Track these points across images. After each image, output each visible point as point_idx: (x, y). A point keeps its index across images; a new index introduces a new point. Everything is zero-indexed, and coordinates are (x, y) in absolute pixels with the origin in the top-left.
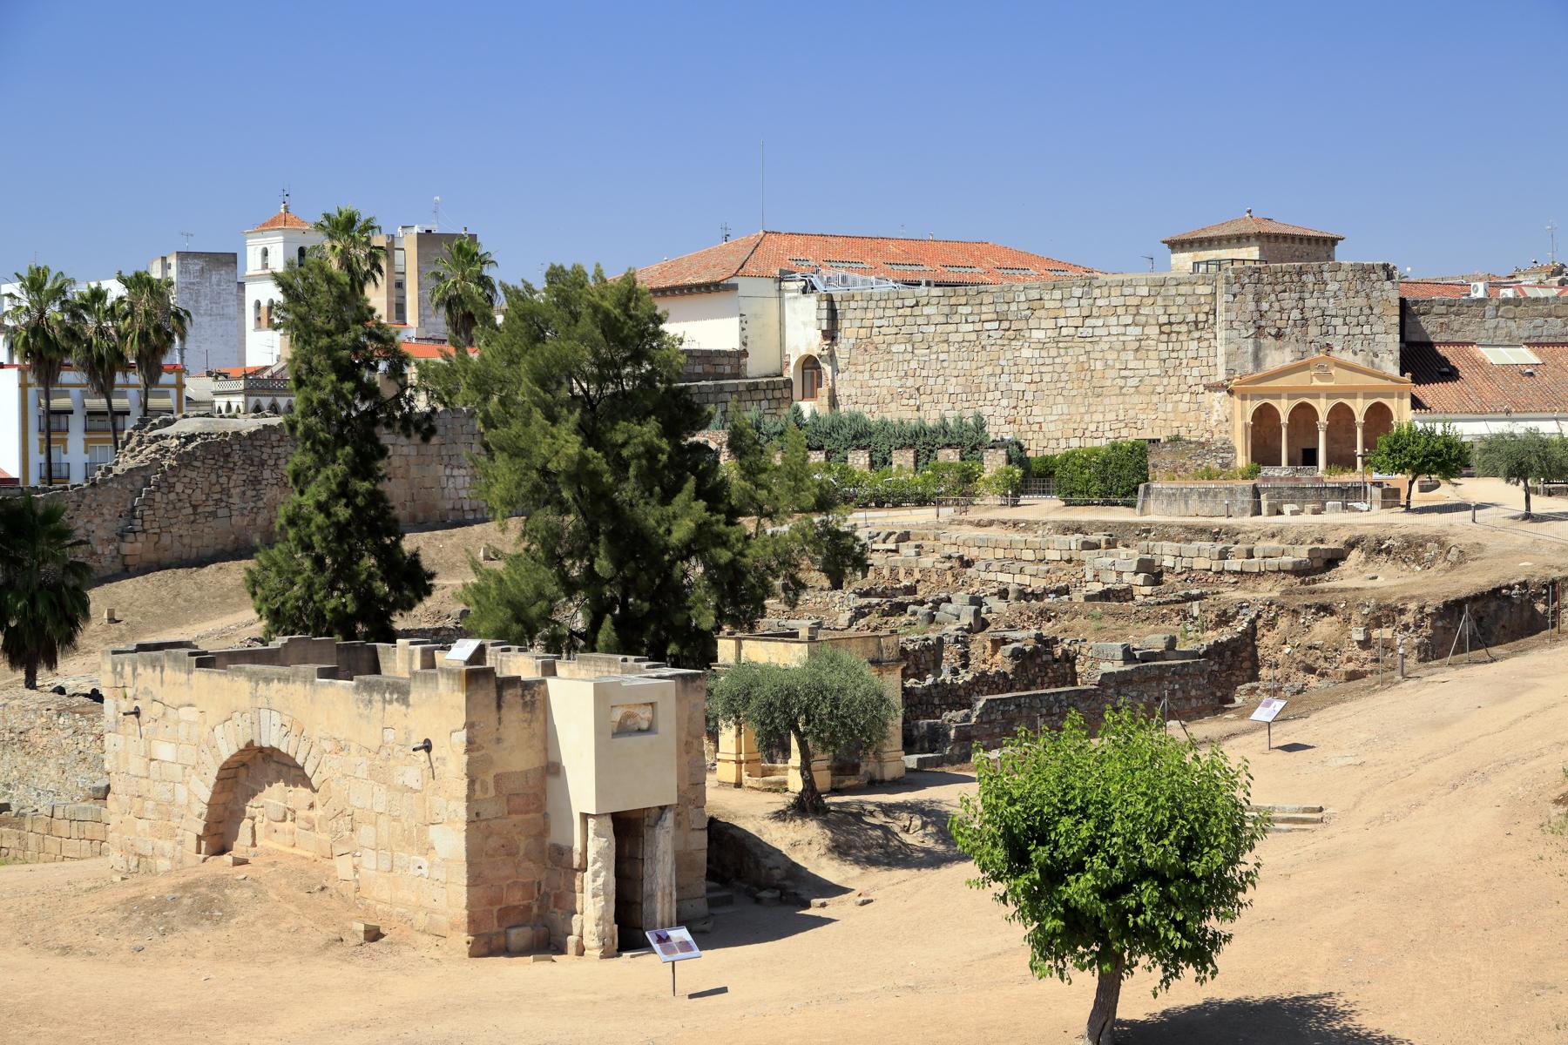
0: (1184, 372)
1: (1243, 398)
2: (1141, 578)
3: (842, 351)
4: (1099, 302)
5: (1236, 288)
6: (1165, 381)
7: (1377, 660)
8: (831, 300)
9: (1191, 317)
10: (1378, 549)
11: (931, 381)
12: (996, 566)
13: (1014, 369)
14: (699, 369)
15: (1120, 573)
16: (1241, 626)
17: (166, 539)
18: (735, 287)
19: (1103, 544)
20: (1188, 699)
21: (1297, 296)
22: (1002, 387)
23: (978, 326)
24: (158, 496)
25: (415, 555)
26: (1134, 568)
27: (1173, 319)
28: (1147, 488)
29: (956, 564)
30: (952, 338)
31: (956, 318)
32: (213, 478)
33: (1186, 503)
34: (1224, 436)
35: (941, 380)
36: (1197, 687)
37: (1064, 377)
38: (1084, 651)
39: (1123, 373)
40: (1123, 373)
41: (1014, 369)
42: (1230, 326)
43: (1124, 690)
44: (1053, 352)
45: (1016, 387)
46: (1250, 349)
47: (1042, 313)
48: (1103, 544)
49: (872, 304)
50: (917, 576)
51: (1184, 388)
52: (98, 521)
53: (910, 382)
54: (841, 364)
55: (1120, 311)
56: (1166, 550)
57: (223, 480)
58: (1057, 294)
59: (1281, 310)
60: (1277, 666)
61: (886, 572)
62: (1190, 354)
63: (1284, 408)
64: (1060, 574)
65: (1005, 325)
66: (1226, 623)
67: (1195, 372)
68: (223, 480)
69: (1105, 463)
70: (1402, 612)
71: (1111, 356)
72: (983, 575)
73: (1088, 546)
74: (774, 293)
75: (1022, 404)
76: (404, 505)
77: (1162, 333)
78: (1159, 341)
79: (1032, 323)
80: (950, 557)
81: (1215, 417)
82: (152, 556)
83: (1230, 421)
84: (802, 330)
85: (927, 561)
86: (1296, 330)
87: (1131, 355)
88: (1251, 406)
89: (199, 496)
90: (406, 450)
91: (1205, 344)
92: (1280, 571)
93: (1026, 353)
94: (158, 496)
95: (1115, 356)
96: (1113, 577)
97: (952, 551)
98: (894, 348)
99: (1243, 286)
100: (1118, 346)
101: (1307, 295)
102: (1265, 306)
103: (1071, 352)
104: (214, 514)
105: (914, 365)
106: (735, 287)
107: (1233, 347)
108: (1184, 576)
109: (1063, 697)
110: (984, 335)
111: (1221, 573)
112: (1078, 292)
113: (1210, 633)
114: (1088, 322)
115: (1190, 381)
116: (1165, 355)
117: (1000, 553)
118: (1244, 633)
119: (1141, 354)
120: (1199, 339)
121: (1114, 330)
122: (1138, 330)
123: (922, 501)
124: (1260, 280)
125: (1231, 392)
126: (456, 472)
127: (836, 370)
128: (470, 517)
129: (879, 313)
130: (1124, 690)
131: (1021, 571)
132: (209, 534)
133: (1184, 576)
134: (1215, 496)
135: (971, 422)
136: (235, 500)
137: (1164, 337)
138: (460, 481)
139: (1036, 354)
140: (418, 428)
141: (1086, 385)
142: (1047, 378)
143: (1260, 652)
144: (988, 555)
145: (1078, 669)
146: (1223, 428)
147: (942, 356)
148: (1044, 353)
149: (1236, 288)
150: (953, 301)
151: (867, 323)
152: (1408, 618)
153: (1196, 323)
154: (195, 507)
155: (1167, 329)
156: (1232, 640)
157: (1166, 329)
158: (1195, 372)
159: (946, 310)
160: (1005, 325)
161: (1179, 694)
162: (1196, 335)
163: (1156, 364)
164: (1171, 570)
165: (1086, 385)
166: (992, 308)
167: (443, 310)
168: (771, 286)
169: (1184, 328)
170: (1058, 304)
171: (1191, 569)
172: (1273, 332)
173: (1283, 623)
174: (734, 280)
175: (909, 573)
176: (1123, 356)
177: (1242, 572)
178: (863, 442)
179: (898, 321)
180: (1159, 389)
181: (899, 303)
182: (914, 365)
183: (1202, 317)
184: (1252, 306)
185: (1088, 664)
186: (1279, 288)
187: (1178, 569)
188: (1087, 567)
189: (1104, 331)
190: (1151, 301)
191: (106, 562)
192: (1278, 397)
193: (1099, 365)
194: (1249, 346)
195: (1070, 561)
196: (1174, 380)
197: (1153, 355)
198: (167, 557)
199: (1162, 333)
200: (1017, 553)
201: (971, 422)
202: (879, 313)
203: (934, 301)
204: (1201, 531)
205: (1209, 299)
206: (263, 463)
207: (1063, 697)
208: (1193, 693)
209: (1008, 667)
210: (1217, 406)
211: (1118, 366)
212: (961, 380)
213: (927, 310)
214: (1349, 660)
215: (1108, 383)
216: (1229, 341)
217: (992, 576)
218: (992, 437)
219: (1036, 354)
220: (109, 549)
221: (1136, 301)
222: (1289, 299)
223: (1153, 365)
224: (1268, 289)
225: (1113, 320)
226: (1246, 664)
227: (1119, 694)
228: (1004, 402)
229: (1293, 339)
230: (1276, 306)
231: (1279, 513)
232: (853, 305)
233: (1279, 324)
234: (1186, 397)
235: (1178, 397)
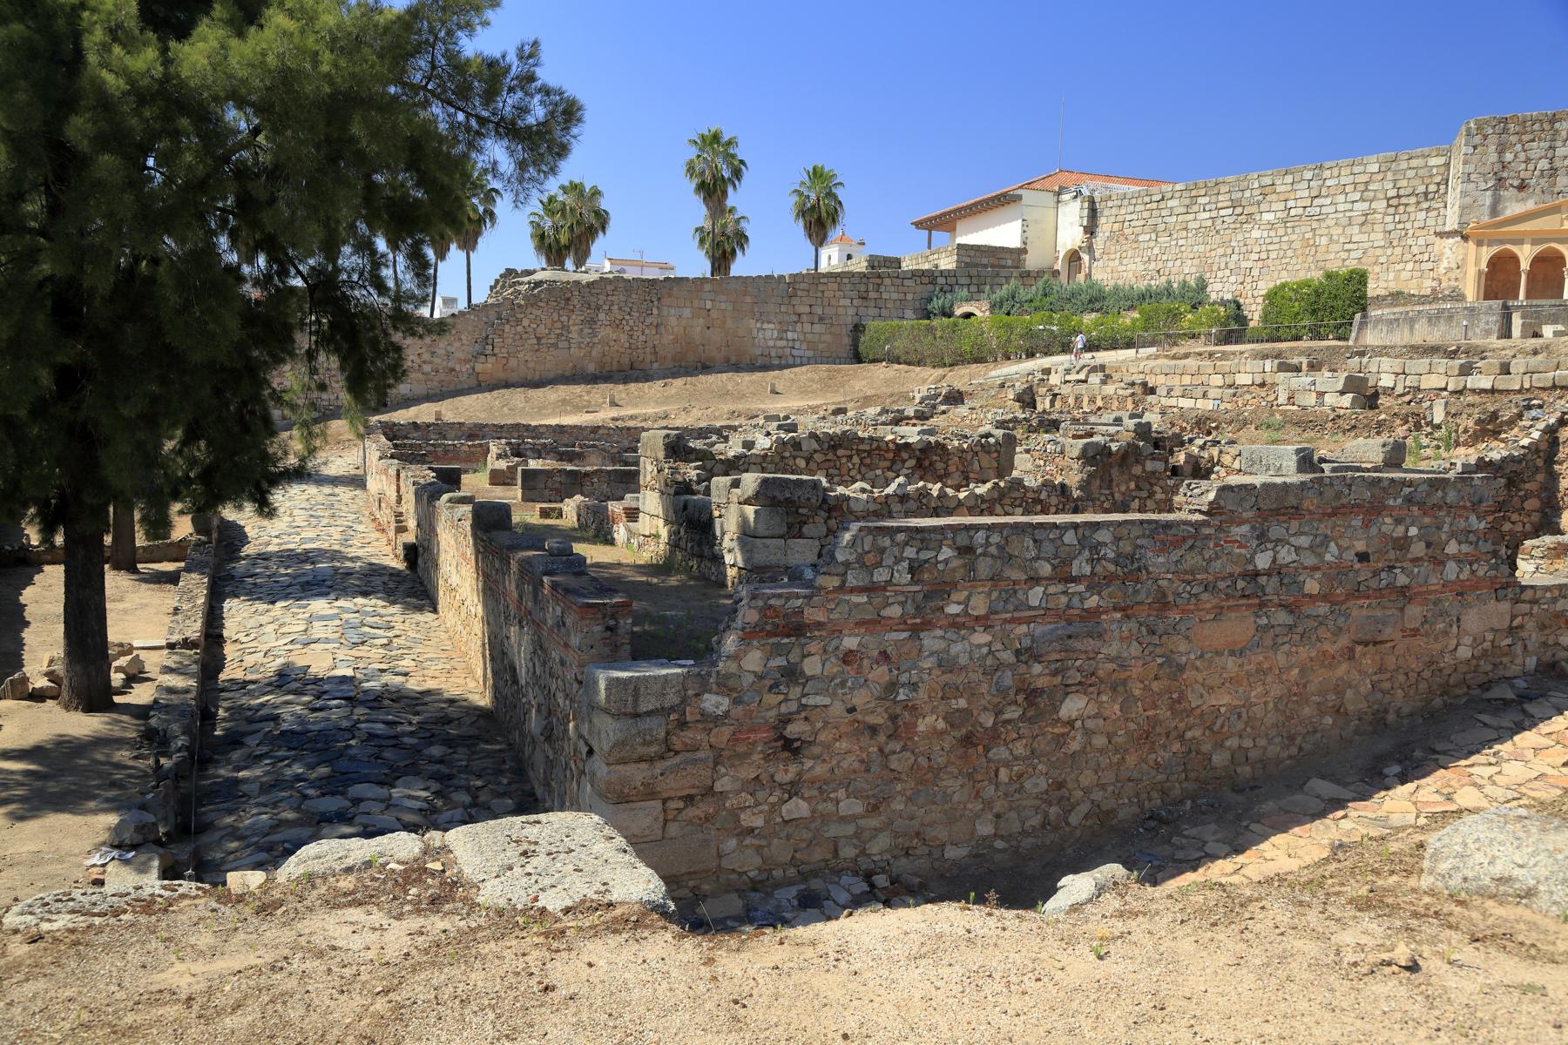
0: (1410, 242)
1: (1479, 244)
2: (1347, 400)
3: (1099, 243)
4: (1328, 183)
5: (1477, 140)
6: (1389, 252)
8: (1092, 201)
9: (1422, 189)
11: (1170, 264)
12: (1177, 392)
13: (1244, 249)
14: (985, 261)
15: (1321, 394)
16: (1528, 436)
17: (513, 363)
18: (1020, 198)
19: (1304, 367)
20: (1439, 562)
21: (1547, 144)
22: (1231, 266)
23: (1214, 214)
24: (507, 327)
26: (1340, 386)
27: (1402, 192)
28: (1364, 317)
29: (1138, 390)
30: (1192, 225)
31: (1195, 208)
32: (555, 316)
33: (1412, 328)
34: (1453, 283)
35: (1178, 263)
36: (1463, 536)
37: (1289, 253)
38: (1227, 459)
39: (1347, 247)
40: (1347, 247)
41: (1244, 249)
42: (1468, 178)
43: (1276, 531)
44: (1281, 232)
45: (1244, 264)
46: (1488, 202)
47: (1274, 197)
48: (1304, 367)
49: (1126, 202)
50: (1099, 403)
51: (1408, 257)
52: (457, 344)
53: (1153, 266)
54: (1097, 255)
55: (1348, 189)
56: (1384, 367)
57: (564, 319)
58: (1289, 179)
59: (1528, 161)
61: (1071, 401)
62: (1417, 224)
63: (1525, 255)
64: (1248, 397)
65: (1238, 210)
66: (1495, 434)
67: (1421, 241)
68: (564, 319)
69: (1318, 294)
71: (1336, 231)
72: (1163, 401)
73: (1284, 367)
74: (1053, 204)
75: (1249, 280)
76: (719, 349)
77: (1389, 206)
78: (1386, 214)
79: (1264, 207)
80: (1133, 384)
81: (1444, 264)
82: (501, 375)
83: (1463, 266)
84: (1070, 233)
85: (1109, 389)
86: (1542, 181)
87: (1356, 229)
88: (1487, 253)
89: (542, 330)
90: (723, 306)
91: (1434, 213)
92: (1554, 387)
93: (1256, 234)
94: (507, 327)
95: (1340, 230)
96: (1311, 400)
97: (1138, 379)
98: (1141, 238)
99: (1485, 137)
100: (1344, 221)
101: (1559, 144)
102: (1509, 156)
103: (1297, 230)
104: (555, 346)
105: (1156, 251)
106: (1020, 198)
107: (1468, 200)
108: (1407, 398)
109: (1104, 536)
110: (1219, 221)
111: (1459, 393)
112: (1308, 175)
113: (1461, 450)
114: (1316, 202)
115: (1415, 250)
116: (1391, 227)
117: (1187, 380)
118: (1533, 449)
119: (1367, 228)
120: (1428, 210)
121: (1341, 208)
122: (1366, 205)
123: (1129, 345)
124: (1505, 131)
125: (1465, 238)
127: (1093, 259)
128: (791, 361)
129: (1131, 208)
130: (1276, 531)
131: (1205, 395)
132: (551, 361)
133: (1407, 398)
134: (1450, 318)
135: (1193, 283)
136: (574, 335)
137: (1392, 210)
138: (768, 334)
139: (1265, 234)
141: (1310, 259)
142: (1273, 255)
144: (1175, 381)
146: (1453, 275)
147: (1181, 242)
148: (1272, 233)
149: (1477, 140)
150: (1194, 193)
151: (1120, 218)
153: (1426, 194)
154: (539, 339)
155: (1395, 203)
156: (1510, 459)
157: (1394, 202)
158: (1421, 241)
159: (1187, 201)
160: (1238, 210)
161: (1418, 549)
162: (1425, 205)
163: (1381, 236)
164: (1389, 391)
165: (1310, 259)
166: (1227, 196)
168: (1050, 198)
169: (1413, 200)
170: (1289, 188)
171: (1418, 389)
172: (1516, 183)
174: (1019, 192)
175: (1092, 400)
176: (1348, 230)
177: (1493, 391)
178: (1097, 306)
179: (1146, 215)
180: (1383, 260)
181: (1147, 199)
182: (1156, 251)
183: (1432, 188)
184: (1493, 157)
186: (1526, 138)
187: (1399, 390)
188: (1281, 388)
189: (1332, 209)
190: (1380, 177)
191: (463, 378)
192: (1520, 242)
193: (1324, 241)
194: (1488, 199)
195: (1262, 385)
196: (1398, 251)
197: (1378, 228)
198: (513, 377)
199: (1389, 206)
200: (1204, 378)
201: (1193, 283)
202: (1131, 208)
203: (1177, 195)
204: (1432, 350)
205: (1442, 170)
206: (598, 308)
207: (1104, 536)
208: (1452, 548)
209: (1073, 477)
210: (1448, 252)
211: (1342, 240)
212: (1196, 262)
213: (1171, 203)
215: (1332, 256)
216: (1464, 194)
217: (1173, 402)
218: (1213, 296)
219: (1265, 234)
220: (466, 368)
221: (1364, 178)
222: (1537, 149)
223: (1378, 238)
224: (1513, 139)
225: (1341, 198)
226: (1532, 504)
227: (1262, 537)
228: (1233, 279)
229: (1538, 190)
230: (1522, 156)
231: (1537, 335)
232: (1110, 204)
233: (1522, 175)
234: (1410, 266)
235: (1401, 266)
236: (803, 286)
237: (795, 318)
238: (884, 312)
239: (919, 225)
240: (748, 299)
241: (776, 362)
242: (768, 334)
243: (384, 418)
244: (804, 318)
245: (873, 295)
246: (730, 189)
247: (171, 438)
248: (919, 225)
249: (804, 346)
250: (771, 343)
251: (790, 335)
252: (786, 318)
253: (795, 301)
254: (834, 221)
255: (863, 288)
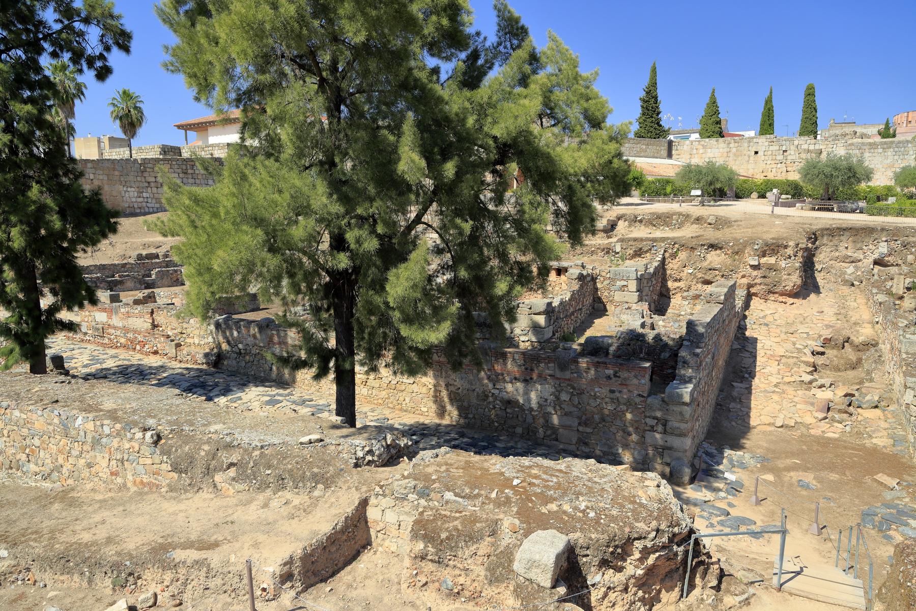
7: (764, 277)
10: (635, 220)
25: (96, 193)
60: (680, 280)
70: (786, 247)
90: (101, 177)
126: (129, 189)
138: (131, 194)
140: (91, 64)
143: (668, 272)
145: (599, 285)
152: (789, 251)
167: (118, 122)
173: (683, 255)
185: (607, 282)
214: (743, 277)
236: (149, 165)
237: (147, 185)
238: (197, 181)
239: (179, 127)
240: (116, 173)
241: (138, 211)
242: (131, 194)
243: (194, 189)
244: (152, 185)
245: (190, 171)
246: (77, 101)
247: (447, 135)
248: (179, 127)
249: (154, 201)
250: (134, 200)
251: (145, 195)
252: (141, 185)
253: (146, 174)
254: (141, 124)
255: (184, 167)
